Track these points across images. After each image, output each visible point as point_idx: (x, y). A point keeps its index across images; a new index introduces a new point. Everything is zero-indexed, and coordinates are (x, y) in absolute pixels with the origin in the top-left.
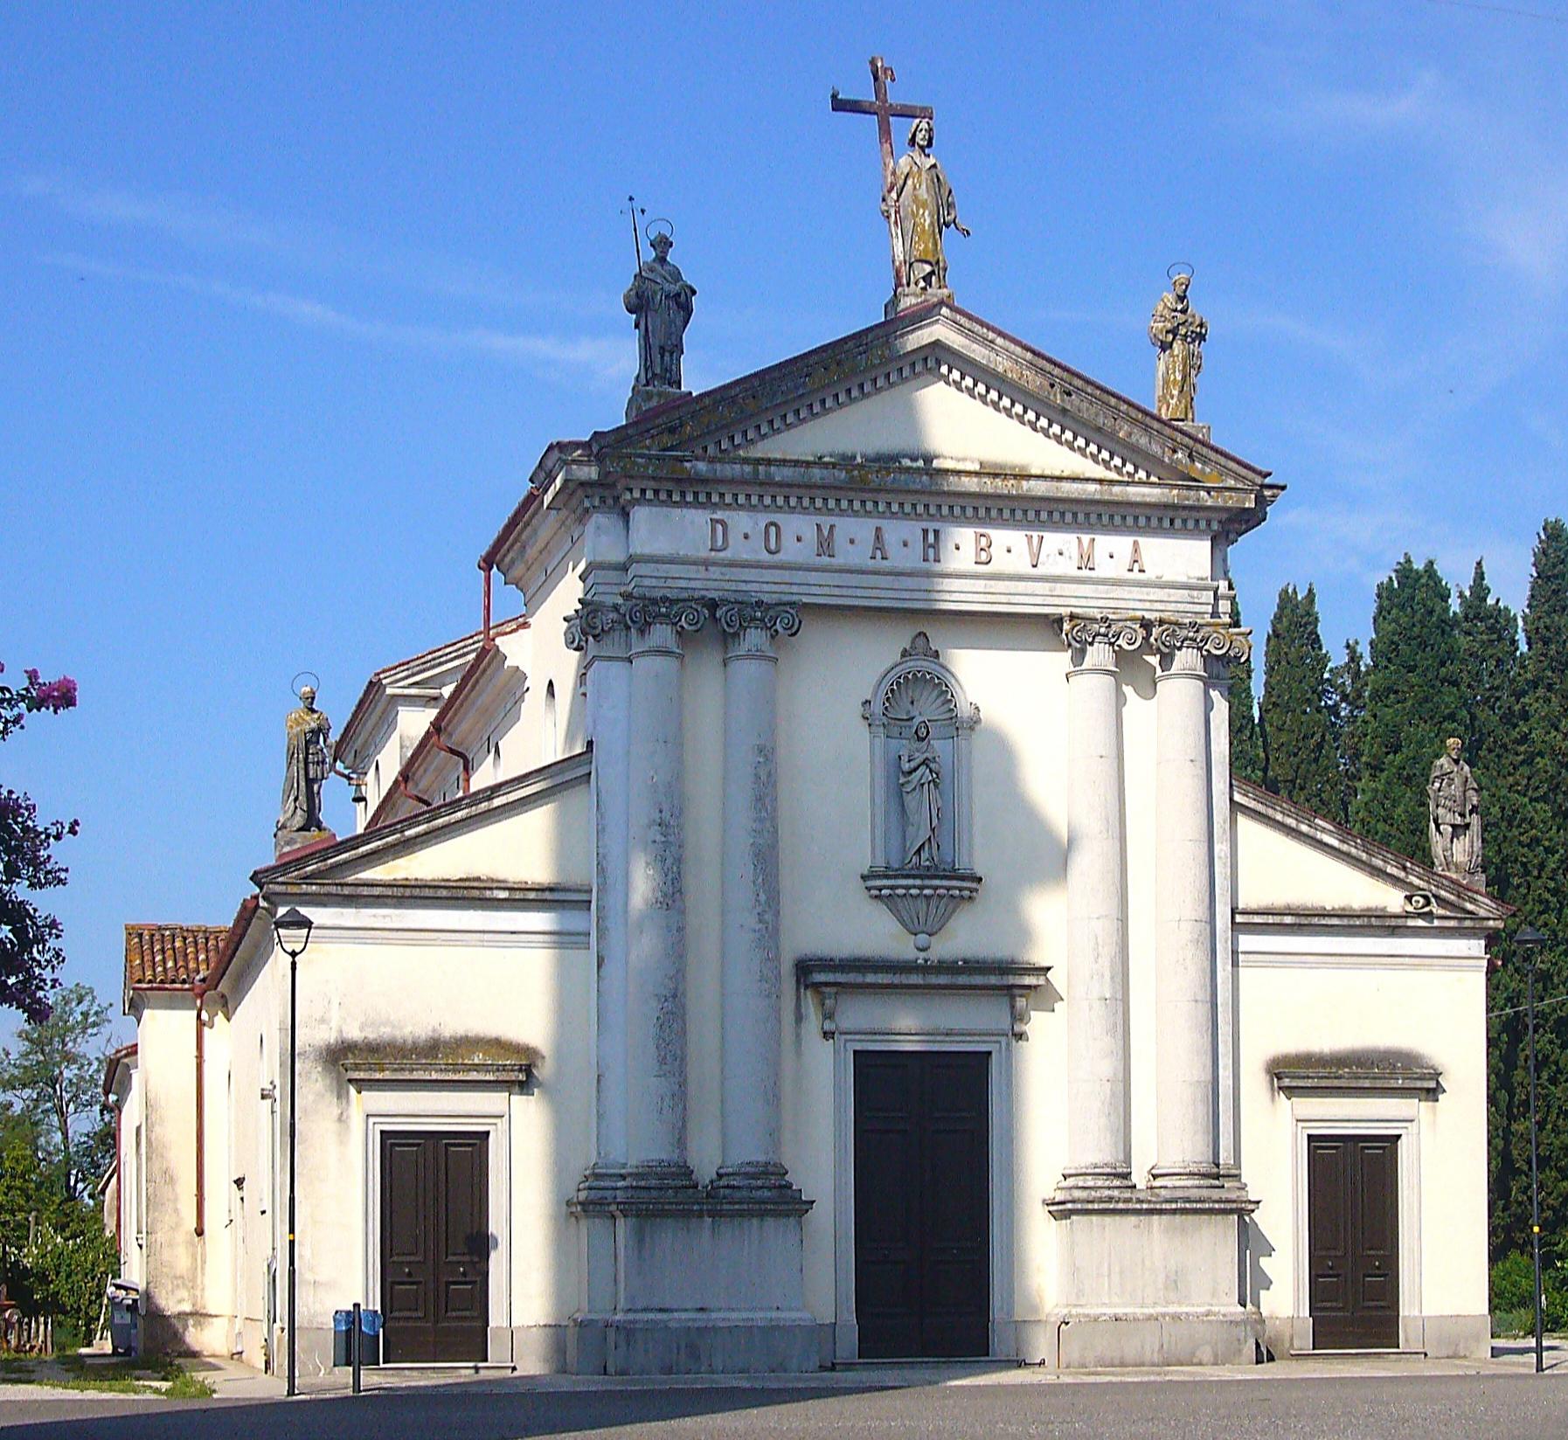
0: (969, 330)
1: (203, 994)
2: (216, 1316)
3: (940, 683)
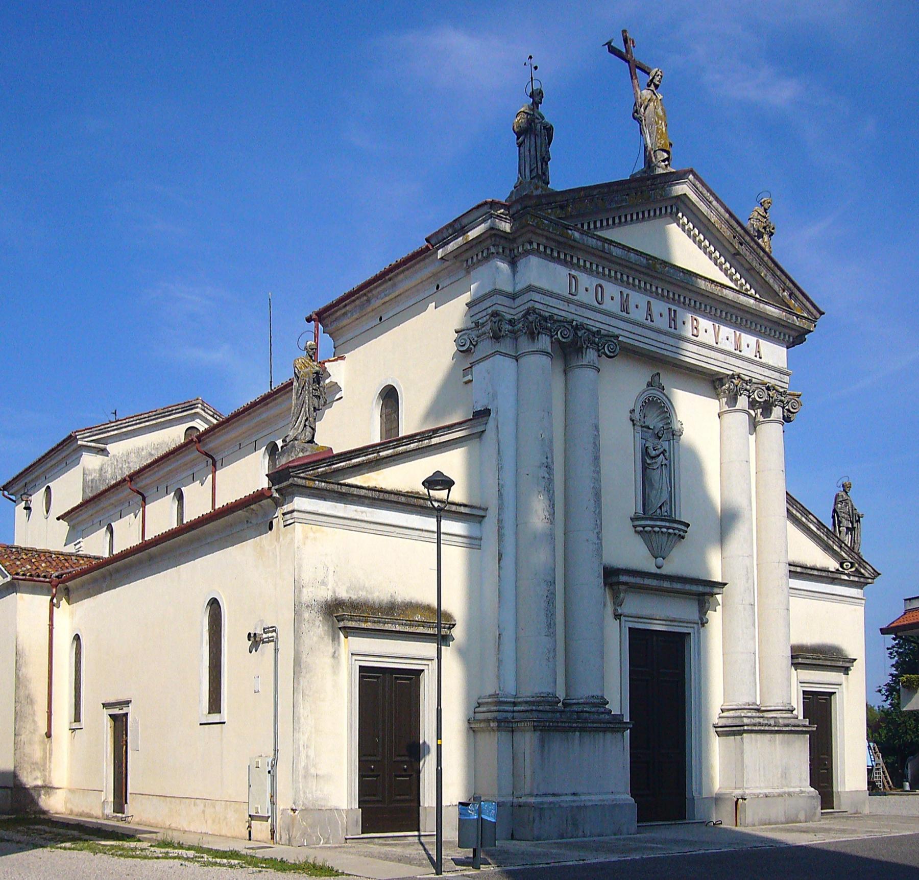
0: (700, 192)
1: (57, 585)
2: (58, 788)
3: (664, 406)
